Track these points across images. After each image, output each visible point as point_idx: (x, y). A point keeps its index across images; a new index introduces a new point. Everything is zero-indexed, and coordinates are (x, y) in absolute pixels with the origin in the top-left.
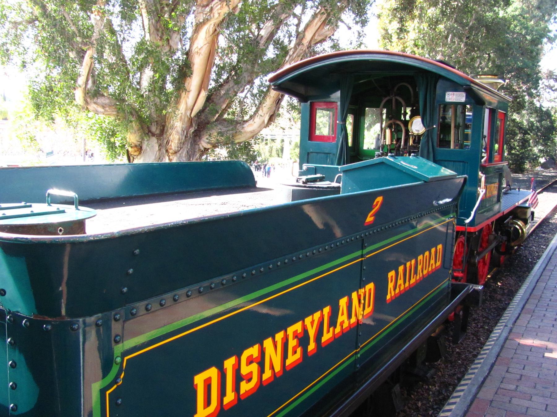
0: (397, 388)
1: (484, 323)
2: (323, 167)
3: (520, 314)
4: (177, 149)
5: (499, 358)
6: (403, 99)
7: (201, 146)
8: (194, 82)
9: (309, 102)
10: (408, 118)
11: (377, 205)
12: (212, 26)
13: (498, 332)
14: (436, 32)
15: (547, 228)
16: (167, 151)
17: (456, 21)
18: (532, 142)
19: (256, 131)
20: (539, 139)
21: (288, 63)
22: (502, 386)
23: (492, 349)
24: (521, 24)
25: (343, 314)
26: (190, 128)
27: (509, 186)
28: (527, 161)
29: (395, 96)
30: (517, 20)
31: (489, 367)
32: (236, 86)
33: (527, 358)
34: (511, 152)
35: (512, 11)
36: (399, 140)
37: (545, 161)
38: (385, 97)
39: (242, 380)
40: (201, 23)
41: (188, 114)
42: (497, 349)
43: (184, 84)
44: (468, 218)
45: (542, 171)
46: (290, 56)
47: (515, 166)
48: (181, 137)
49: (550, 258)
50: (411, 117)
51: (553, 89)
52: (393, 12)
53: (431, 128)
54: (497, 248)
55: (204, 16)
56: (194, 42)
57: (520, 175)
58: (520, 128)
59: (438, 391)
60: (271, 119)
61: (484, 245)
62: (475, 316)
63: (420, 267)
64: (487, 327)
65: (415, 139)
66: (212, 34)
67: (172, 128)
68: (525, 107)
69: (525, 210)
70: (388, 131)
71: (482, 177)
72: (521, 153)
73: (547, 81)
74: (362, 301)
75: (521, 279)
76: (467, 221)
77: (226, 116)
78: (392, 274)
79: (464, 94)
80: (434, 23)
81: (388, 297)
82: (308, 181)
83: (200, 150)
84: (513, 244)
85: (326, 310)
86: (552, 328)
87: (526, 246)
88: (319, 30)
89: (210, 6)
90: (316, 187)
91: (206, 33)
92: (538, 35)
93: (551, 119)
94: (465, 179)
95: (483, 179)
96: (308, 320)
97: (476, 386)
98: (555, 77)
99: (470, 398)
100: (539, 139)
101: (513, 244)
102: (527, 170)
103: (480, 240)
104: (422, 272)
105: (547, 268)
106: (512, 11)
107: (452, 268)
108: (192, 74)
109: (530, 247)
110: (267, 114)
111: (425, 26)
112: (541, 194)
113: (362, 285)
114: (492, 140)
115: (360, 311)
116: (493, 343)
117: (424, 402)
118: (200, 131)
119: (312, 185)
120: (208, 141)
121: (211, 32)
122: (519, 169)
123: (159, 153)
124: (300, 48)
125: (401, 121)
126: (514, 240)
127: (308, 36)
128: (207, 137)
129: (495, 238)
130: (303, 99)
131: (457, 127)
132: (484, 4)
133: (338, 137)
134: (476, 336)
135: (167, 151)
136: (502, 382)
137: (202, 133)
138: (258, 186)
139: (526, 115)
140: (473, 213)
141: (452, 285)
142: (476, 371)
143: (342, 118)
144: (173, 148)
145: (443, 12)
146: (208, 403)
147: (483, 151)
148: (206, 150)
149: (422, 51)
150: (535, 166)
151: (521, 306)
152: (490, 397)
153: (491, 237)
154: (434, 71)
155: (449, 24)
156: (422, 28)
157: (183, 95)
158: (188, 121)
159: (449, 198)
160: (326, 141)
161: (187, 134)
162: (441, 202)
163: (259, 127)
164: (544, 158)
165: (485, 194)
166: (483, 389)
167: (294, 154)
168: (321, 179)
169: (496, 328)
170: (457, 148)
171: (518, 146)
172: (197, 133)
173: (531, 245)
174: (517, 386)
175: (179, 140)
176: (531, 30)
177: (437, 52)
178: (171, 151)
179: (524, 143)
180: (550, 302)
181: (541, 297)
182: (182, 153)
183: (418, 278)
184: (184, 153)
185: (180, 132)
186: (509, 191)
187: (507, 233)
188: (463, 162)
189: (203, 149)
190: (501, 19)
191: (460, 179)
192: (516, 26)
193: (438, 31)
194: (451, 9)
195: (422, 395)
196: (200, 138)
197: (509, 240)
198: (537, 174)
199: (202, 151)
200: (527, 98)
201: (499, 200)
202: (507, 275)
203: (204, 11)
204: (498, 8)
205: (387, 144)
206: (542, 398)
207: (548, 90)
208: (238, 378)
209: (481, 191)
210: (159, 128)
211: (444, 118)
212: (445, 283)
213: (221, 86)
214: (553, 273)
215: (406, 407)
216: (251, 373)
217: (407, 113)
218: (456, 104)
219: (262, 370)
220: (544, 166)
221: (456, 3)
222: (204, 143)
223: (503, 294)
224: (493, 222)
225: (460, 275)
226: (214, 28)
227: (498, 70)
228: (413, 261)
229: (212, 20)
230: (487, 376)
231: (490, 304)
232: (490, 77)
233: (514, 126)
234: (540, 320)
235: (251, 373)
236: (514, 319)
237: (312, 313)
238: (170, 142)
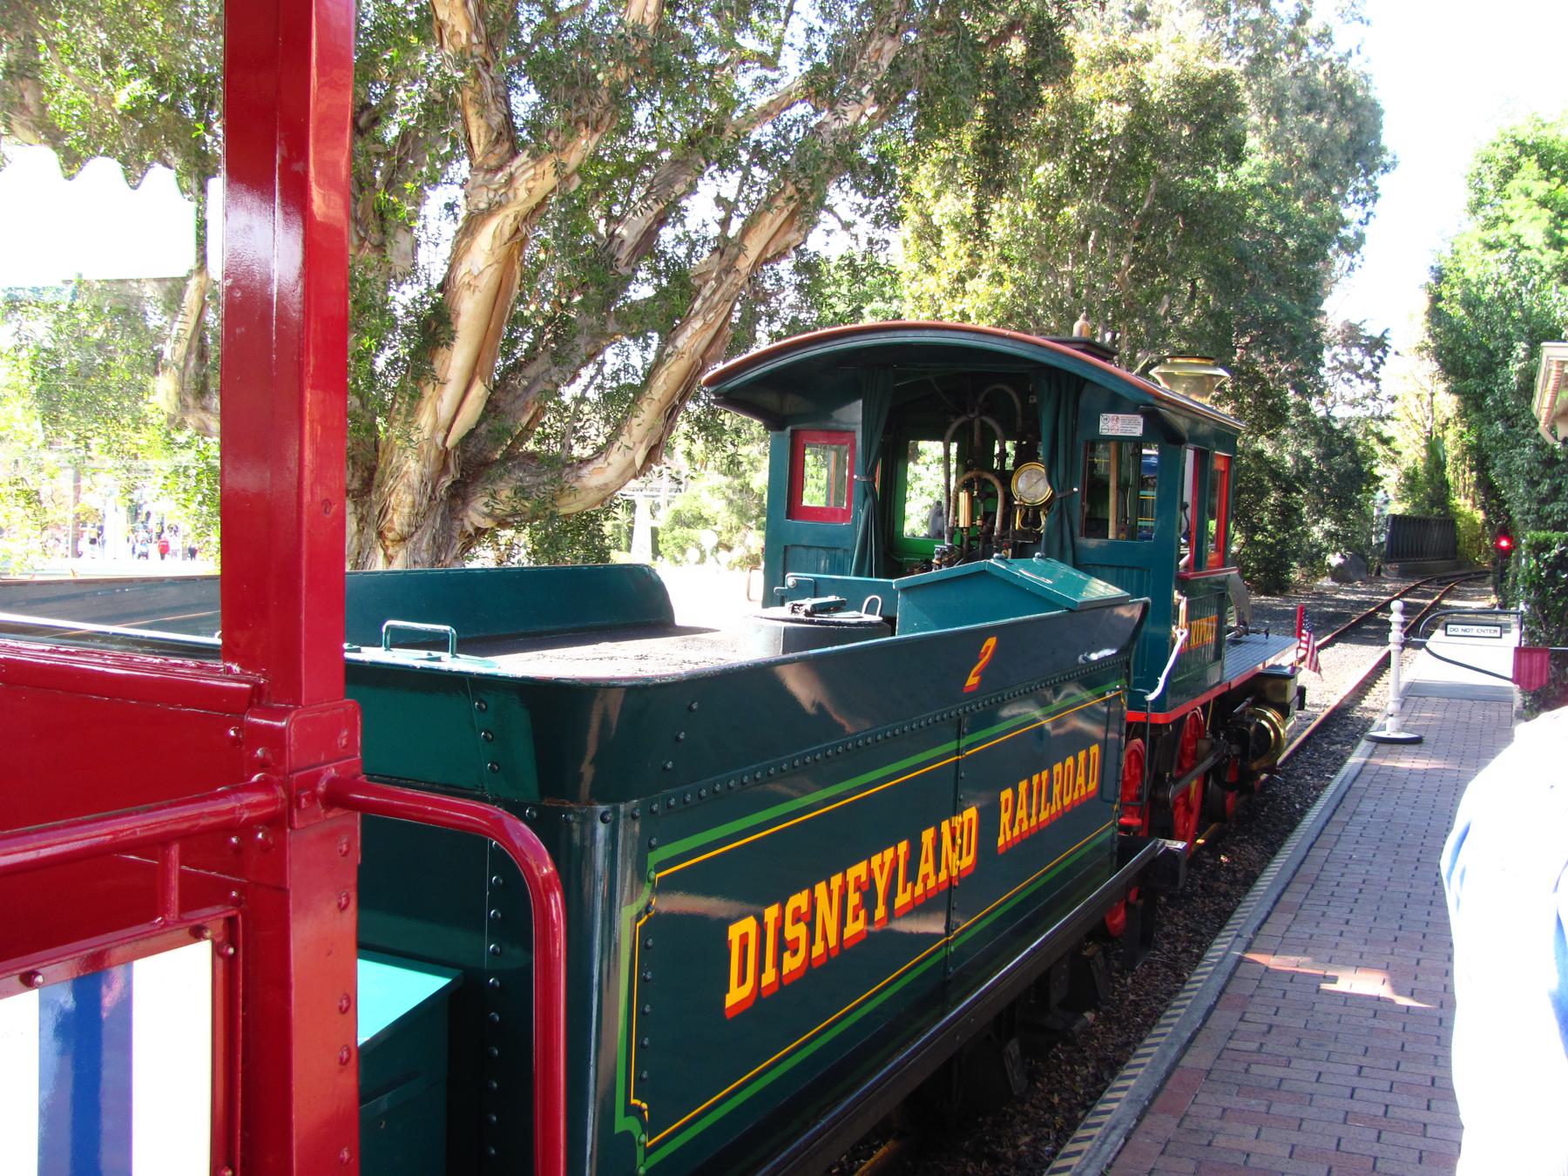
0: (1013, 1047)
1: (1190, 941)
2: (834, 580)
3: (1269, 914)
4: (406, 529)
5: (1224, 996)
6: (998, 422)
7: (466, 523)
8: (457, 359)
9: (789, 429)
10: (1010, 462)
11: (985, 653)
12: (512, 217)
13: (1222, 948)
14: (1056, 223)
15: (1341, 733)
16: (380, 534)
17: (1106, 198)
18: (1308, 512)
19: (612, 485)
20: (1326, 504)
21: (700, 317)
22: (1231, 1045)
23: (1209, 980)
24: (1272, 209)
25: (926, 861)
26: (440, 477)
27: (1245, 624)
28: (1295, 564)
29: (981, 414)
30: (1262, 197)
31: (1202, 1013)
32: (554, 370)
33: (1284, 994)
34: (1252, 538)
35: (1250, 175)
36: (989, 516)
37: (1341, 561)
38: (958, 416)
39: (786, 949)
40: (482, 212)
41: (439, 441)
42: (1220, 980)
43: (431, 363)
44: (1152, 691)
45: (1334, 588)
46: (705, 300)
47: (1265, 576)
48: (418, 498)
49: (1343, 797)
50: (1017, 464)
51: (1361, 372)
52: (943, 169)
53: (1068, 493)
54: (1214, 771)
55: (491, 195)
56: (461, 258)
57: (1276, 600)
58: (1276, 475)
59: (1095, 1075)
60: (653, 455)
61: (1187, 765)
62: (1168, 928)
63: (1056, 789)
64: (1196, 951)
65: (1027, 514)
66: (509, 240)
67: (397, 473)
68: (1287, 419)
69: (1284, 682)
70: (963, 497)
71: (1180, 601)
72: (1278, 542)
73: (1344, 351)
74: (959, 841)
75: (1273, 849)
76: (1151, 697)
77: (530, 446)
78: (1007, 794)
79: (1141, 420)
80: (1051, 202)
81: (1001, 841)
82: (816, 609)
83: (463, 532)
84: (1255, 766)
85: (903, 847)
86: (1338, 939)
87: (1289, 775)
88: (778, 237)
89: (507, 170)
90: (834, 623)
91: (494, 237)
92: (1313, 236)
93: (1354, 453)
94: (1146, 605)
95: (1183, 607)
96: (876, 860)
97: (1176, 1048)
98: (1363, 342)
99: (1163, 1068)
100: (1326, 504)
101: (1255, 766)
102: (1297, 586)
103: (1177, 752)
104: (1062, 799)
105: (1334, 818)
106: (1250, 175)
107: (1119, 800)
108: (453, 339)
109: (1299, 778)
110: (641, 442)
111: (1028, 208)
112: (1330, 649)
113: (957, 810)
114: (1204, 509)
115: (953, 858)
116: (1211, 968)
117: (1066, 1096)
118: (466, 485)
119: (825, 617)
120: (486, 510)
121: (507, 234)
122: (1274, 581)
123: (359, 539)
124: (729, 280)
125: (993, 471)
126: (1257, 757)
127: (754, 248)
128: (486, 500)
129: (1213, 747)
130: (774, 422)
131: (1122, 488)
132: (1178, 157)
133: (857, 512)
134: (1173, 969)
135: (380, 534)
136: (1230, 1038)
137: (470, 489)
138: (680, 620)
139: (1290, 442)
140: (1162, 680)
141: (1121, 838)
142: (1176, 1020)
143: (867, 466)
144: (397, 527)
145: (1074, 175)
146: (742, 980)
147: (1183, 541)
148: (480, 532)
149: (1020, 274)
150: (1316, 576)
151: (1273, 896)
152: (1205, 1063)
153: (1204, 745)
154: (1077, 371)
155: (1088, 204)
156: (1021, 214)
157: (428, 391)
158: (437, 458)
159: (1111, 647)
160: (828, 519)
161: (433, 491)
162: (1094, 657)
163: (619, 477)
164: (1338, 554)
165: (1188, 639)
166: (1192, 1051)
167: (671, 543)
168: (838, 607)
169: (1218, 940)
170: (1122, 535)
171: (1271, 523)
172: (456, 489)
173: (1300, 772)
174: (1261, 1045)
175: (413, 507)
176: (1295, 224)
177: (1058, 275)
178: (390, 535)
179: (1288, 516)
180: (1336, 889)
181: (1317, 878)
182: (420, 540)
183: (1053, 811)
184: (425, 540)
185: (417, 485)
186: (1244, 637)
187: (1242, 738)
188: (1139, 568)
189: (471, 530)
190: (1223, 195)
191: (1131, 612)
192: (1259, 213)
193: (1062, 223)
194: (1094, 167)
195: (1059, 1082)
196: (465, 503)
197: (1244, 755)
198: (1321, 595)
199: (470, 535)
200: (1292, 397)
201: (1218, 656)
202: (1242, 841)
203: (490, 182)
204: (1215, 166)
205: (961, 525)
206: (1310, 1063)
207: (1346, 375)
208: (783, 945)
209: (1180, 634)
210: (359, 474)
211: (1093, 466)
212: (1105, 832)
213: (518, 367)
214: (1347, 828)
215: (1027, 1106)
216: (797, 939)
217: (1007, 455)
218: (1120, 441)
219: (811, 941)
220: (1339, 574)
221: (1108, 153)
222: (476, 515)
223: (1233, 883)
224: (1209, 702)
225: (1136, 821)
226: (515, 224)
227: (1217, 325)
228: (1045, 774)
229: (510, 205)
230: (1199, 1030)
231: (1203, 902)
232: (1195, 361)
233: (1260, 470)
234: (1314, 924)
235: (797, 939)
236: (1257, 923)
237: (881, 849)
238: (390, 511)
